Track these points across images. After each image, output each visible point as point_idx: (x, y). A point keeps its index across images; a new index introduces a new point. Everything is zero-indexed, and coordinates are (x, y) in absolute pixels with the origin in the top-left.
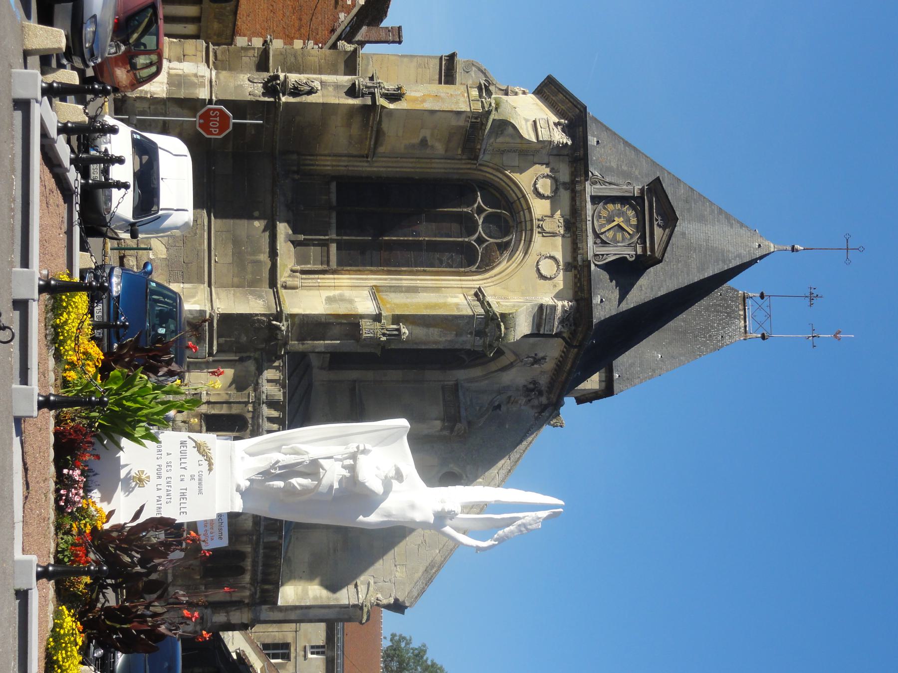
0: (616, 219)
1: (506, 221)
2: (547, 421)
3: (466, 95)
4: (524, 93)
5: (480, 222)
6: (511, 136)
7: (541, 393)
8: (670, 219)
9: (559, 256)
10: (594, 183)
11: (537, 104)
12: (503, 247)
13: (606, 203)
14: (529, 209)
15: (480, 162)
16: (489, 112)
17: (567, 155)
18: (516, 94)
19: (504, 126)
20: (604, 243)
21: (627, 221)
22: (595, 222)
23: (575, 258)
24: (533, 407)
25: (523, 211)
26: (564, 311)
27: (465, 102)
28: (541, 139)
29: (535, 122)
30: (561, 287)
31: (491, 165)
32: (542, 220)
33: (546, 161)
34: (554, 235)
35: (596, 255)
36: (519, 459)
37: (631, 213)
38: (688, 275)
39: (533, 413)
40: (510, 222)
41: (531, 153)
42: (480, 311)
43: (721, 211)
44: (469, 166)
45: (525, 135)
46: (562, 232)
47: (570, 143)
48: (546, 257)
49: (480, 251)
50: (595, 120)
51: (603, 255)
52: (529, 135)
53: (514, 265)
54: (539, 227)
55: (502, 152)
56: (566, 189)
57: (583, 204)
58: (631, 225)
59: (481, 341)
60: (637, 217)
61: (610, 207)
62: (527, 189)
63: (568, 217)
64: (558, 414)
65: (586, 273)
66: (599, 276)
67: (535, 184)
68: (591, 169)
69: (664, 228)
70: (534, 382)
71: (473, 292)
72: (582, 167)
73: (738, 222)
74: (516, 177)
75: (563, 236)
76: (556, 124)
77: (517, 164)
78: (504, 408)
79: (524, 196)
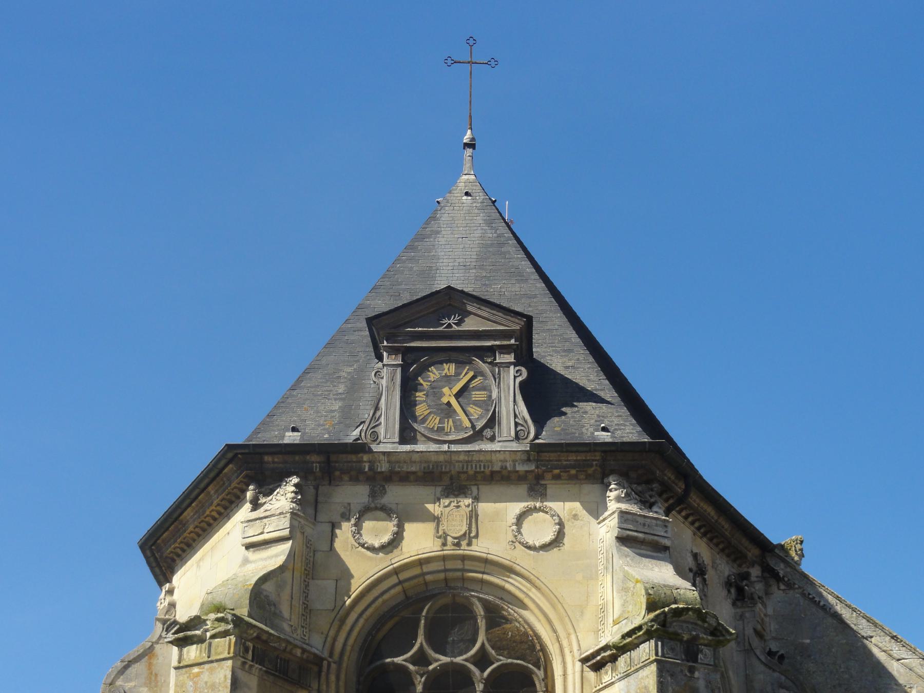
0: (445, 400)
1: (444, 608)
2: (793, 566)
3: (196, 670)
4: (171, 592)
5: (445, 659)
6: (280, 587)
7: (746, 576)
8: (450, 301)
9: (517, 508)
10: (375, 438)
11: (201, 559)
12: (495, 617)
13: (415, 418)
14: (421, 562)
15: (326, 654)
16: (237, 621)
17: (317, 488)
18: (172, 605)
19: (260, 595)
20: (492, 422)
21: (448, 380)
22: (450, 438)
24: (767, 593)
25: (423, 574)
26: (628, 498)
27: (211, 671)
28: (286, 532)
29: (249, 547)
30: (577, 505)
31: (332, 633)
32: (445, 536)
33: (328, 528)
34: (473, 516)
35: (517, 438)
36: (869, 620)
37: (434, 374)
38: (535, 296)
39: (778, 594)
40: (444, 601)
41: (312, 559)
42: (647, 650)
43: (410, 247)
44: (333, 678)
45: (279, 561)
46: (468, 501)
47: (295, 480)
48: (519, 532)
49: (504, 660)
50: (256, 432)
51: (516, 424)
52: (276, 556)
53: (534, 593)
54: (458, 545)
55: (307, 611)
56: (384, 492)
57: (416, 457)
58: (457, 374)
59: (706, 650)
60: (441, 363)
61: (421, 410)
63: (439, 489)
64: (782, 547)
65: (553, 456)
66: (555, 431)
67: (371, 549)
68: (350, 440)
69: (466, 314)
70: (728, 584)
71: (591, 675)
72: (343, 457)
73: (427, 223)
74: (357, 585)
75: (477, 499)
76: (256, 505)
77: (330, 584)
78: (774, 646)
79: (396, 572)
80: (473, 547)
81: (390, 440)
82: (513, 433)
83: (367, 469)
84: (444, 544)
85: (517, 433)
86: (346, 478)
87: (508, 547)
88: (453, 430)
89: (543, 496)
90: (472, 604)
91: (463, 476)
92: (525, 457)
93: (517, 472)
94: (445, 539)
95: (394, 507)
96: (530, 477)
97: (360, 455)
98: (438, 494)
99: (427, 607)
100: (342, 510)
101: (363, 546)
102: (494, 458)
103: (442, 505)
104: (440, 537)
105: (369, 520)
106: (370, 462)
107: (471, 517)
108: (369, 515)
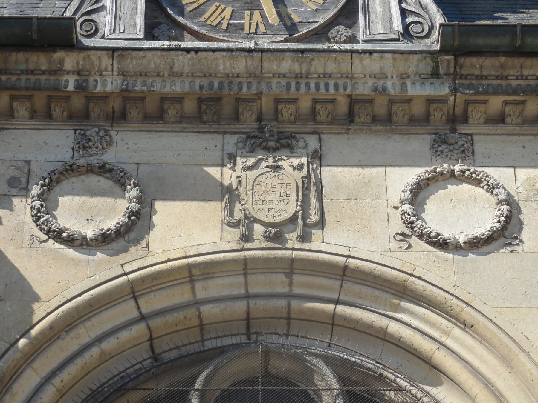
9: (405, 177)
23: (420, 121)
34: (311, 188)
51: (404, 13)
62: (98, 273)
63: (231, 141)
75: (317, 157)
79: (134, 291)
80: (314, 245)
81: (122, 36)
82: (398, 26)
83: (71, 87)
84: (247, 238)
85: (406, 27)
86: (22, 110)
87: (394, 245)
88: (262, 29)
89: (467, 153)
90: (309, 373)
91: (287, 111)
92: (426, 67)
93: (409, 100)
94: (250, 230)
95: (130, 169)
96: (438, 116)
97: (59, 55)
98: (230, 148)
99: (204, 375)
100: (12, 172)
101: (57, 235)
102: (358, 68)
103: (239, 167)
104: (236, 224)
105: (73, 192)
106: (79, 73)
107: (306, 189)
108: (74, 181)
